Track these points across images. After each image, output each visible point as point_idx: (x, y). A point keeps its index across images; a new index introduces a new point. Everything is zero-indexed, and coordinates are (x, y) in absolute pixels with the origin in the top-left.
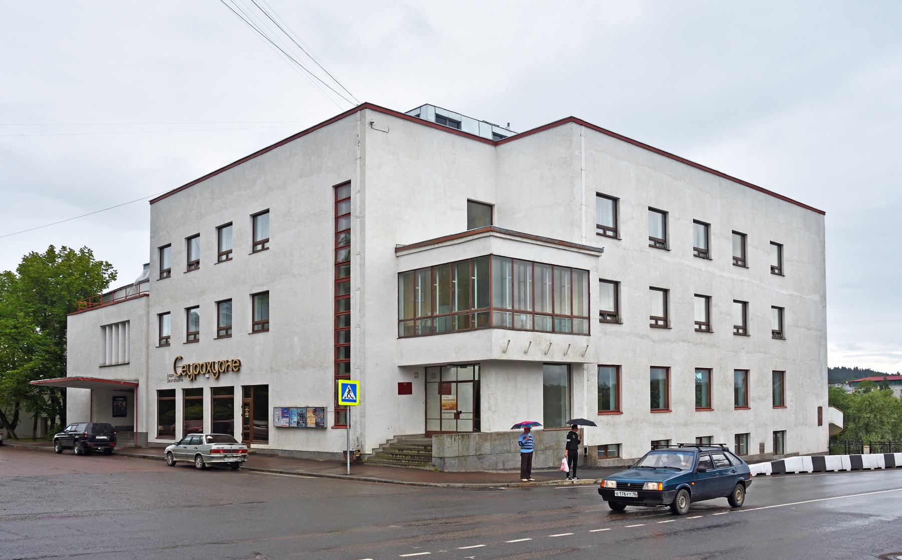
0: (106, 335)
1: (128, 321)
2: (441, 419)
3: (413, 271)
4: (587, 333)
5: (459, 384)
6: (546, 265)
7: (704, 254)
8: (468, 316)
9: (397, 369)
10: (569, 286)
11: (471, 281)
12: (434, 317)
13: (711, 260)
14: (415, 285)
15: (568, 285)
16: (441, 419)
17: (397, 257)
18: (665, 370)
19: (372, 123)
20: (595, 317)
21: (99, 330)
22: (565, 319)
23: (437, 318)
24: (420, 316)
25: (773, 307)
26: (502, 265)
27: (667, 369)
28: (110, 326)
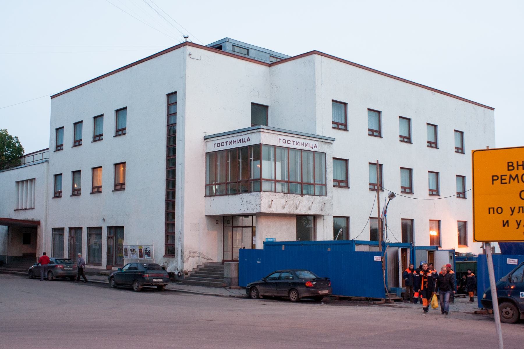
0: (19, 189)
1: (35, 179)
2: (232, 252)
3: (215, 152)
4: (325, 195)
5: (243, 228)
6: (284, 148)
7: (407, 139)
9: (204, 217)
10: (313, 163)
12: (227, 183)
13: (438, 148)
16: (232, 252)
18: (346, 219)
19: (190, 55)
20: (330, 183)
21: (15, 184)
22: (271, 182)
23: (230, 184)
25: (493, 184)
26: (281, 151)
27: (348, 218)
28: (22, 182)
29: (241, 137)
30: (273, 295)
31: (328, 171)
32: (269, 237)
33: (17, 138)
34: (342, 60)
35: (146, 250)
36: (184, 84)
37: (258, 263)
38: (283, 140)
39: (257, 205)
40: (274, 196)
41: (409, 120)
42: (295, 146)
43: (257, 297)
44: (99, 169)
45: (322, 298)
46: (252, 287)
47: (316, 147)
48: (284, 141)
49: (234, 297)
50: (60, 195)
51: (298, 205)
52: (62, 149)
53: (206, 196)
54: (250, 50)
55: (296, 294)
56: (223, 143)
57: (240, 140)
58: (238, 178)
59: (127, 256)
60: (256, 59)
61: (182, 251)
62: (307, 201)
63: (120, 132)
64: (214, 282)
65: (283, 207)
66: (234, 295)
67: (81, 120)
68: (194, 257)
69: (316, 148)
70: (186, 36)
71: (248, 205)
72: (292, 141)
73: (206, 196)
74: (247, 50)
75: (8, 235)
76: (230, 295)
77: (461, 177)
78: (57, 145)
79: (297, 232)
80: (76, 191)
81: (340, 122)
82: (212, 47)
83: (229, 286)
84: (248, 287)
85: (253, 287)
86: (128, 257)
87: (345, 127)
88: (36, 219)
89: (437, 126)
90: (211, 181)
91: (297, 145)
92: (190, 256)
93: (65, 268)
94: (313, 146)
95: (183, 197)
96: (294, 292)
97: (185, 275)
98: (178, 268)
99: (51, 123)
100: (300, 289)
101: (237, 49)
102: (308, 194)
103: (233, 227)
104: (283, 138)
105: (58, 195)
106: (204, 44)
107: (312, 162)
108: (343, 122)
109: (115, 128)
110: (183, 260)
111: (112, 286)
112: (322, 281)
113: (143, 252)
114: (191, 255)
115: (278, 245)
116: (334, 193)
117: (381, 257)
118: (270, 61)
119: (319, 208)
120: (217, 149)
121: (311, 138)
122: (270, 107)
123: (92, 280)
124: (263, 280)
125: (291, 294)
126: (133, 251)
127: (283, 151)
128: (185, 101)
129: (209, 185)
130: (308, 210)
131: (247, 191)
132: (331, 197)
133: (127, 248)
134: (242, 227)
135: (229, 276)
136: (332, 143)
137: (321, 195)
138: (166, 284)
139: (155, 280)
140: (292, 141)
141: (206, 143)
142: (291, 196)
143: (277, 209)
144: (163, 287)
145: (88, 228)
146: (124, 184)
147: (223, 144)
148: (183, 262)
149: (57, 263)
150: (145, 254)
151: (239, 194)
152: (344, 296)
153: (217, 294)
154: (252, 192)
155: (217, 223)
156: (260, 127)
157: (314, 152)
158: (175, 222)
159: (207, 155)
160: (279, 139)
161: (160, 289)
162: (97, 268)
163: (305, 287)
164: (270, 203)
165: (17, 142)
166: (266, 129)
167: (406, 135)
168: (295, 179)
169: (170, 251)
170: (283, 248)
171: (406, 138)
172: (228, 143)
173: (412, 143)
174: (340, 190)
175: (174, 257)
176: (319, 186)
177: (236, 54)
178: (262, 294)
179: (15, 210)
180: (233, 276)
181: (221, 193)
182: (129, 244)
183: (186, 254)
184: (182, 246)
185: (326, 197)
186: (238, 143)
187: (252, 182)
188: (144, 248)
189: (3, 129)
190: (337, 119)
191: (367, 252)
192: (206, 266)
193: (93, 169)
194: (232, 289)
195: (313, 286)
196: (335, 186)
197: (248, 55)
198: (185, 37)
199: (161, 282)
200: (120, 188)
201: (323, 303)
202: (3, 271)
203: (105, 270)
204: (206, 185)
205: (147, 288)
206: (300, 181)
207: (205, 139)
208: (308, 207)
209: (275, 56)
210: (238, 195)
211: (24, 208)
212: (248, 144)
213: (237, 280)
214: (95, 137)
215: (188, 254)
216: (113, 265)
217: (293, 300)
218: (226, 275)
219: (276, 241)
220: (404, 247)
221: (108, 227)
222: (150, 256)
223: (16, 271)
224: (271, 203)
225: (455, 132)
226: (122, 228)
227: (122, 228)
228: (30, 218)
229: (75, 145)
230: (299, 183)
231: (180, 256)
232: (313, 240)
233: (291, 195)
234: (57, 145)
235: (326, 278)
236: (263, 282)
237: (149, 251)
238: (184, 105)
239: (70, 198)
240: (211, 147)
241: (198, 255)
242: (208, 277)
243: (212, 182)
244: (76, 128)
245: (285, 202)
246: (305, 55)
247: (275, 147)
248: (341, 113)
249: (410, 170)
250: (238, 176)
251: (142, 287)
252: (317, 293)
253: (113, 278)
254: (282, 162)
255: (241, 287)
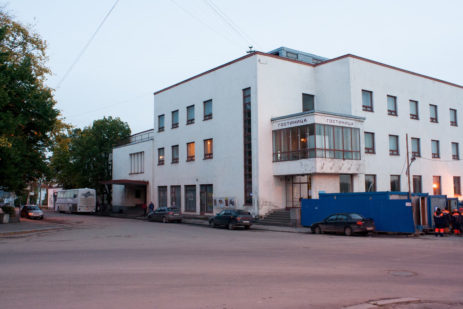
1: (143, 152)
2: (293, 201)
4: (360, 159)
5: (301, 184)
7: (415, 117)
8: (305, 152)
9: (273, 176)
11: (306, 135)
14: (280, 137)
15: (323, 133)
16: (293, 201)
17: (272, 123)
19: (259, 60)
20: (363, 151)
21: (128, 156)
24: (283, 151)
26: (328, 128)
27: (375, 176)
28: (134, 154)
29: (299, 119)
30: (332, 231)
31: (361, 141)
32: (321, 190)
33: (127, 123)
34: (368, 61)
35: (231, 201)
36: (256, 82)
37: (316, 209)
38: (330, 120)
39: (313, 167)
40: (325, 161)
41: (417, 102)
42: (338, 124)
43: (319, 233)
44: (191, 144)
45: (368, 233)
46: (315, 226)
47: (353, 124)
48: (331, 121)
49: (302, 233)
50: (163, 163)
51: (341, 167)
52: (164, 130)
53: (273, 162)
54: (299, 55)
55: (350, 230)
56: (286, 123)
57: (299, 121)
58: (298, 148)
59: (216, 205)
60: (303, 61)
61: (258, 201)
62: (347, 164)
63: (208, 117)
64: (283, 223)
65: (331, 169)
66: (301, 231)
67: (177, 109)
68: (266, 205)
69: (352, 125)
70: (251, 47)
71: (306, 167)
72: (336, 121)
73: (273, 162)
74: (296, 55)
75: (125, 191)
76: (299, 231)
77: (455, 144)
78: (160, 127)
79: (340, 187)
80: (175, 159)
81: (367, 106)
82: (272, 54)
83: (294, 225)
84: (312, 225)
85: (316, 226)
86: (217, 206)
87: (371, 109)
88: (146, 180)
89: (372, 92)
90: (277, 151)
91: (339, 123)
92: (263, 205)
93: (175, 214)
94: (351, 124)
95: (257, 163)
96: (349, 229)
97: (261, 218)
98: (255, 214)
99: (155, 112)
100: (353, 226)
101: (289, 55)
102: (347, 159)
103: (293, 183)
104: (329, 118)
105: (161, 162)
106: (266, 52)
107: (332, 134)
108: (370, 105)
109: (204, 114)
110: (259, 208)
111: (212, 226)
112: (368, 221)
113: (229, 202)
114: (264, 204)
115: (332, 196)
116: (366, 157)
117: (411, 203)
118: (313, 63)
119: (355, 169)
120: (281, 128)
121: (349, 118)
122: (315, 96)
123: (192, 222)
124: (324, 221)
125: (346, 230)
126: (220, 201)
127: (329, 128)
128: (257, 94)
129: (275, 154)
130: (348, 170)
131: (305, 156)
132: (364, 161)
133: (216, 200)
134: (300, 183)
135: (295, 219)
136: (363, 121)
137: (356, 159)
138: (252, 225)
139: (244, 222)
140: (336, 121)
141: (272, 123)
142: (336, 160)
143: (327, 170)
144: (249, 227)
145: (185, 186)
146: (212, 154)
147: (285, 124)
148: (259, 209)
149: (169, 210)
150: (230, 204)
151: (299, 160)
152: (383, 232)
153: (289, 231)
154: (309, 158)
155: (281, 181)
156: (314, 111)
157: (351, 128)
158: (252, 180)
159: (273, 132)
160: (327, 119)
161: (247, 228)
162: (193, 214)
163: (357, 225)
164: (322, 166)
165: (127, 126)
166: (318, 113)
167: (415, 113)
168: (338, 148)
169: (249, 201)
170: (335, 198)
171: (414, 115)
172: (289, 123)
173: (419, 120)
174: (369, 155)
175: (252, 205)
176: (355, 153)
177: (289, 58)
178: (323, 230)
179: (129, 174)
180: (297, 219)
181: (284, 159)
182: (217, 197)
183: (261, 203)
184: (258, 197)
185: (360, 161)
186: (297, 123)
187: (309, 151)
188: (229, 199)
189: (117, 117)
190: (365, 103)
191: (397, 200)
192: (274, 212)
193: (188, 144)
194: (298, 227)
195: (362, 224)
196: (391, 154)
197: (297, 58)
198: (250, 48)
199: (248, 223)
200: (208, 157)
201: (370, 237)
202: (125, 217)
203: (199, 215)
204: (273, 154)
205: (238, 227)
206: (333, 149)
207: (272, 121)
208: (348, 168)
209: (316, 59)
210: (298, 160)
211: (136, 173)
212: (305, 123)
213: (300, 222)
214: (188, 121)
215: (262, 203)
216: (205, 212)
217: (348, 234)
218: (292, 218)
219: (326, 193)
220: (423, 196)
221: (200, 185)
222: (234, 205)
223: (135, 216)
224: (323, 166)
225: (387, 97)
226: (212, 185)
227: (212, 185)
228: (142, 180)
229: (173, 127)
230: (341, 151)
231: (256, 205)
232: (351, 192)
233: (336, 159)
234: (160, 127)
235: (371, 219)
236: (324, 222)
237: (233, 201)
238: (256, 97)
239: (171, 164)
240: (276, 126)
241: (269, 204)
242: (277, 219)
243: (277, 151)
244: (173, 115)
245: (333, 165)
246: (342, 57)
247: (324, 125)
248: (368, 98)
249: (418, 139)
250: (298, 146)
251: (235, 227)
252: (365, 230)
253: (212, 221)
254: (329, 135)
255: (303, 226)
